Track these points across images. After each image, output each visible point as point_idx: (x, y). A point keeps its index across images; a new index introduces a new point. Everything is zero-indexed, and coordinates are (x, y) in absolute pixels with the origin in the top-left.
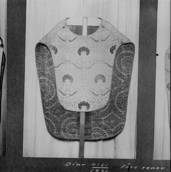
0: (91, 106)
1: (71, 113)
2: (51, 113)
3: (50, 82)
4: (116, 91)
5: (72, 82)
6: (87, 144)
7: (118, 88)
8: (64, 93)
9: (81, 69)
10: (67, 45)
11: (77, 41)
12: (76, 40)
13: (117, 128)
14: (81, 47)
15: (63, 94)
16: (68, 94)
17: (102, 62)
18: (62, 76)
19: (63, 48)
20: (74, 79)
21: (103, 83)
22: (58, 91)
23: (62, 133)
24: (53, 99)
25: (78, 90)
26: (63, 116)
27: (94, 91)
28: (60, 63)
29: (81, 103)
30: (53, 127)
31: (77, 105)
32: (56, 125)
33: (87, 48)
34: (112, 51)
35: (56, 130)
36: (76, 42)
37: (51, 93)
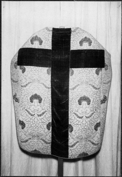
15: (30, 114)
18: (30, 96)
25: (47, 110)
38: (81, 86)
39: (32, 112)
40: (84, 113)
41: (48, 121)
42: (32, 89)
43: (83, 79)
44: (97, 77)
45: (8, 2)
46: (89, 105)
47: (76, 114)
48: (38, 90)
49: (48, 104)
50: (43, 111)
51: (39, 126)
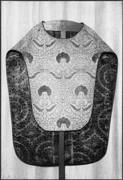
0: (72, 123)
1: (48, 134)
2: (24, 136)
3: (22, 100)
4: (99, 110)
5: (49, 94)
6: (67, 168)
7: (101, 106)
8: (40, 107)
9: (60, 79)
10: (44, 50)
11: (55, 46)
12: (54, 44)
13: (100, 152)
14: (61, 52)
16: (45, 110)
17: (82, 71)
18: (38, 88)
19: (40, 55)
20: (53, 91)
21: (84, 96)
22: (33, 106)
23: (37, 159)
24: (26, 119)
26: (38, 139)
27: (74, 105)
28: (35, 72)
29: (60, 119)
30: (26, 152)
31: (55, 123)
32: (29, 149)
33: (67, 54)
34: (94, 59)
35: (29, 156)
36: (55, 47)
37: (23, 113)
38: (41, 74)
39: (40, 107)
40: (45, 105)
41: (58, 117)
42: (41, 80)
43: (43, 66)
44: (58, 65)
45: (38, 2)
46: (86, 96)
47: (73, 106)
48: (47, 81)
49: (58, 96)
50: (52, 105)
51: (48, 123)
